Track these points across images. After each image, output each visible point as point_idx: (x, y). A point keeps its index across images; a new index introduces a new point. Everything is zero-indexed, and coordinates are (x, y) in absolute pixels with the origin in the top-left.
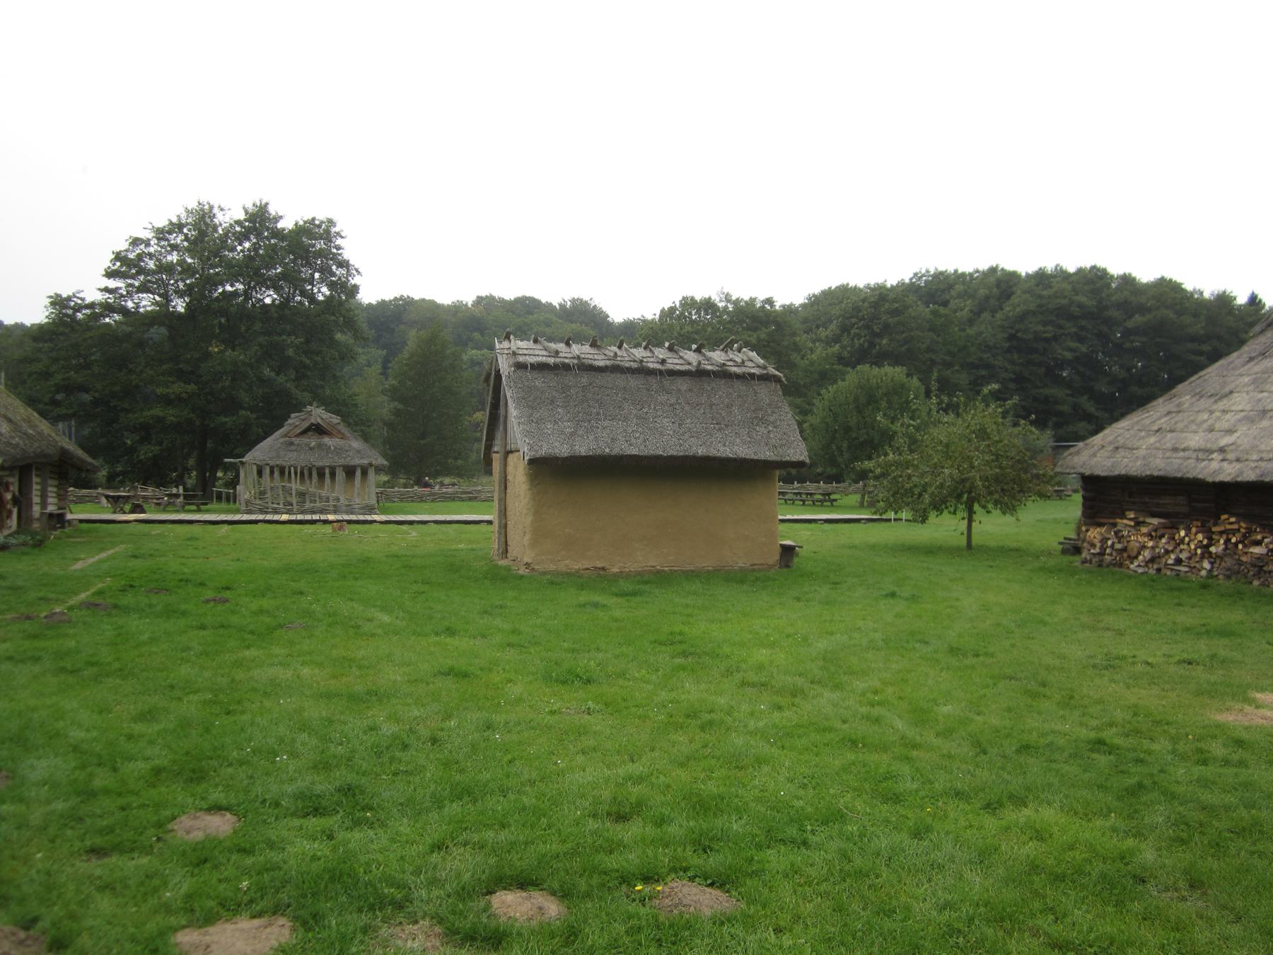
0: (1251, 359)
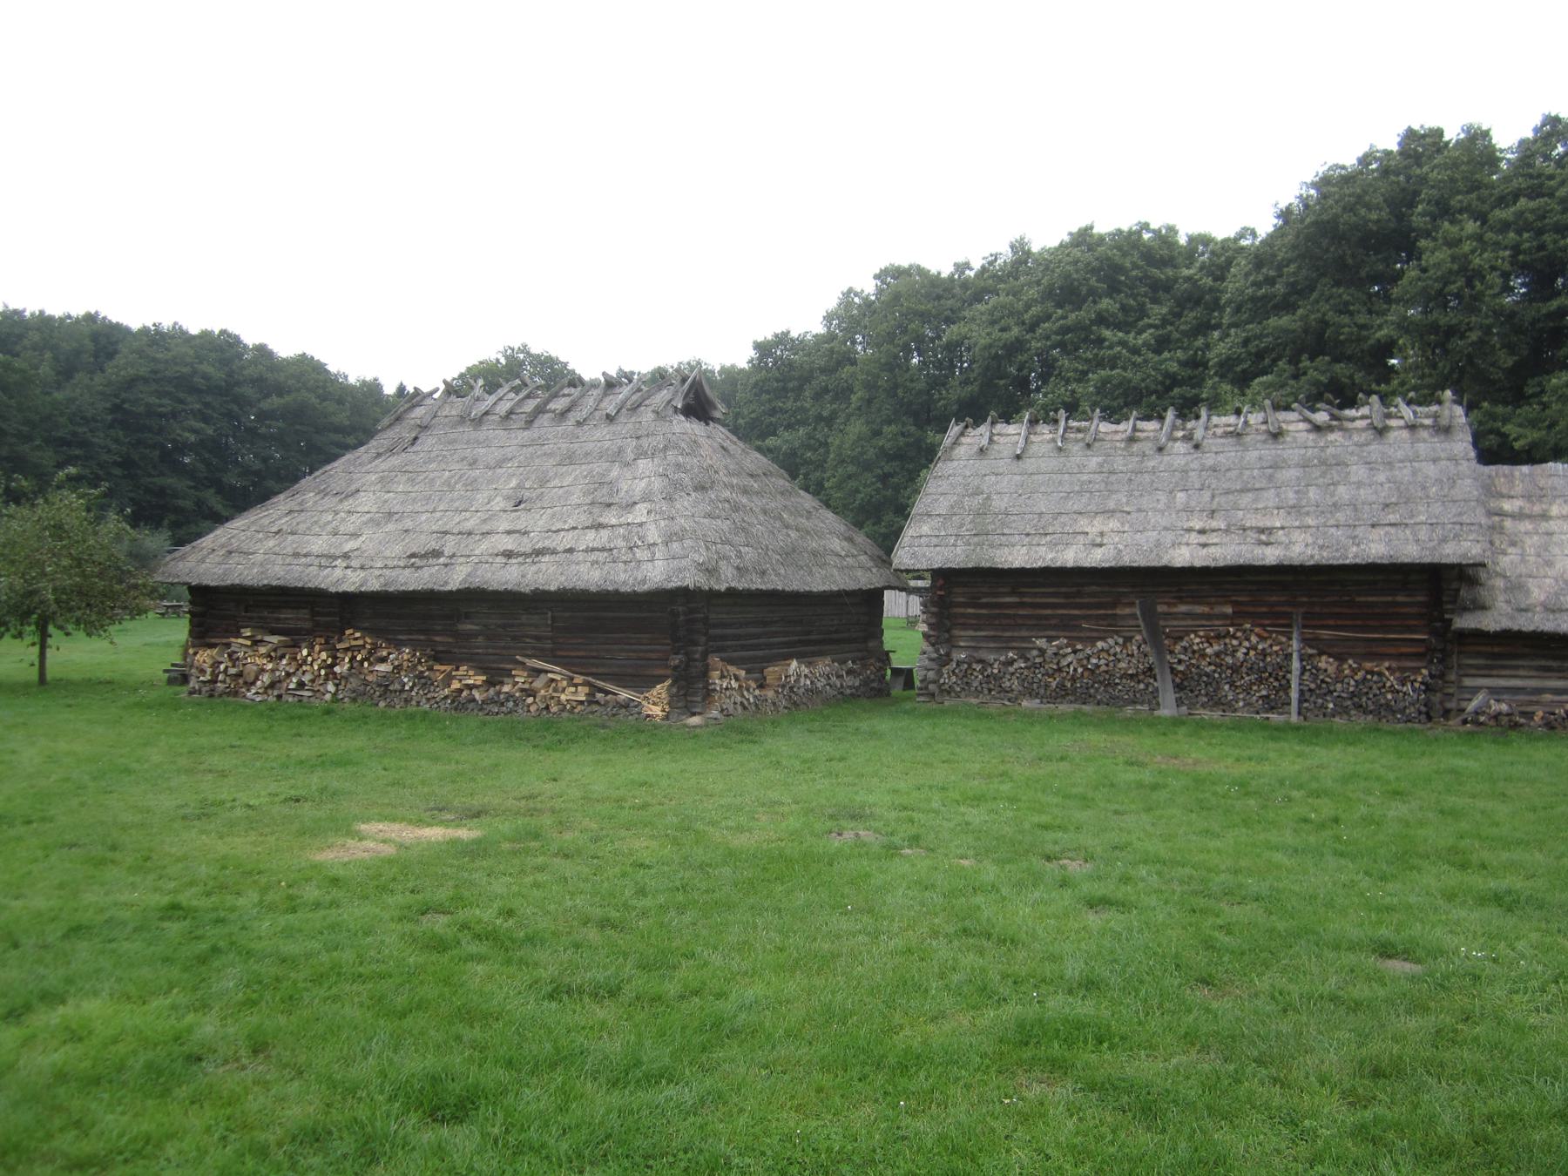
0: (379, 455)
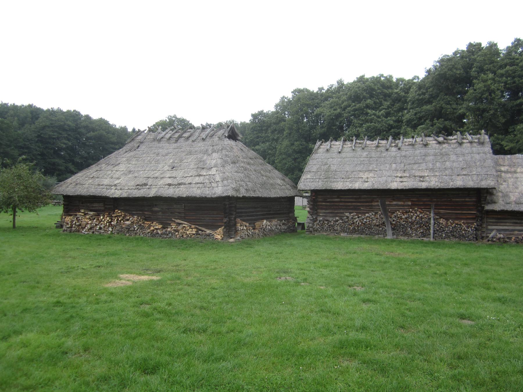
0: (126, 152)
